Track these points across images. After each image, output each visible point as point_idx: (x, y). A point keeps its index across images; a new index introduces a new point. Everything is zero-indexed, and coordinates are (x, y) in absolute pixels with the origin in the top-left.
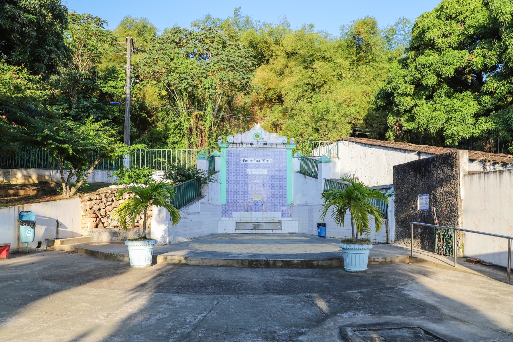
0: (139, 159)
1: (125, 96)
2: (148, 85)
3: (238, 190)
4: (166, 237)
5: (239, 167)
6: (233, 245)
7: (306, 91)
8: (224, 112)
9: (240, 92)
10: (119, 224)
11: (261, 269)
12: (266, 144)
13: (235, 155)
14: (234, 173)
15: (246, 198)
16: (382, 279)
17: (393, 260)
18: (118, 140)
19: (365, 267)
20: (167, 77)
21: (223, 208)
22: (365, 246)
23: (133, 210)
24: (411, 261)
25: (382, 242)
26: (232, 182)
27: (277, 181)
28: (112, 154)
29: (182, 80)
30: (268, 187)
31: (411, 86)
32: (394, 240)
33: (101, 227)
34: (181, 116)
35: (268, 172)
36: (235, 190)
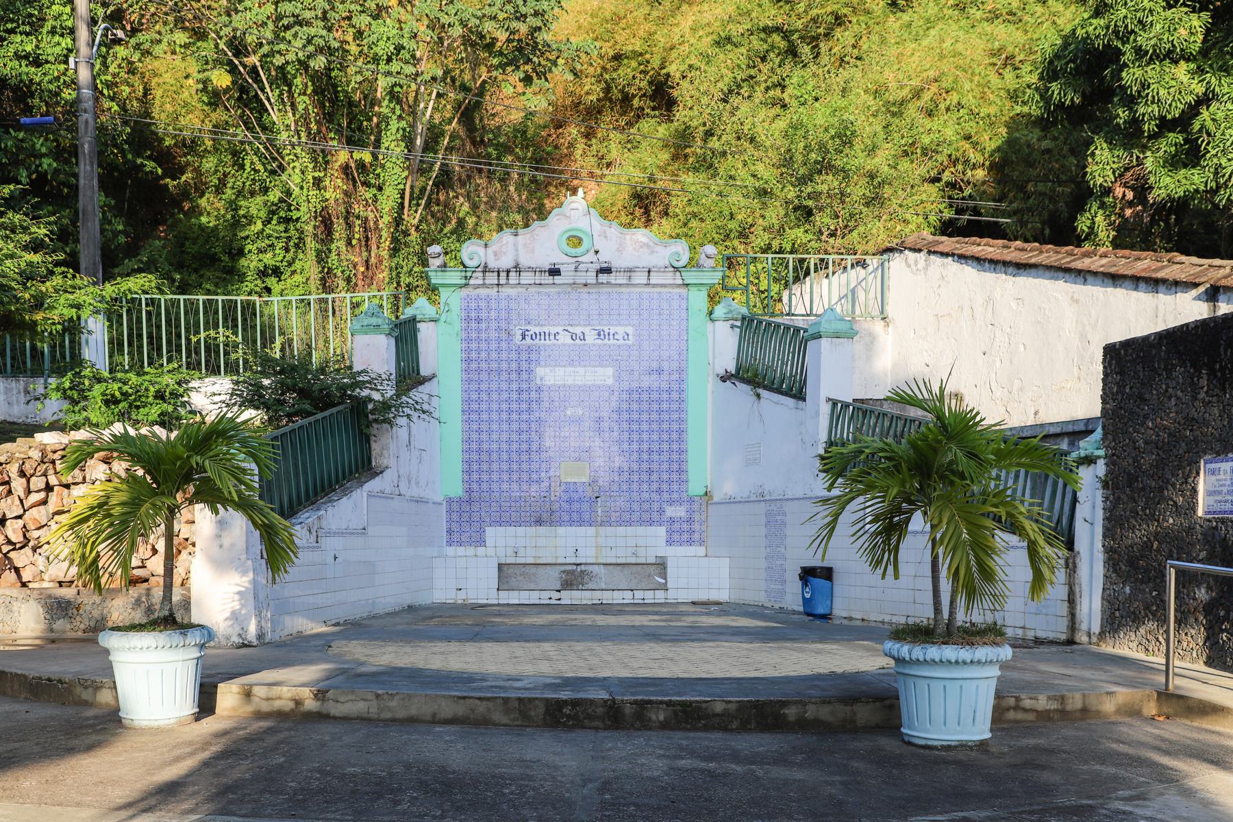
0: (140, 336)
1: (74, 94)
2: (158, 50)
3: (504, 446)
4: (248, 619)
5: (509, 361)
6: (488, 647)
7: (763, 59)
8: (449, 149)
9: (509, 69)
10: (74, 570)
11: (593, 732)
12: (607, 270)
13: (493, 314)
14: (490, 381)
15: (534, 476)
16: (1046, 776)
17: (1093, 703)
18: (57, 264)
19: (980, 731)
20: (229, 15)
21: (450, 511)
22: (982, 652)
23: (122, 522)
24: (1165, 710)
25: (1051, 636)
26: (485, 416)
27: (650, 411)
28: (39, 317)
29: (287, 28)
30: (616, 434)
31: (1194, 16)
32: (1096, 629)
33: (12, 585)
34: (289, 171)
35: (618, 378)
36: (495, 446)
